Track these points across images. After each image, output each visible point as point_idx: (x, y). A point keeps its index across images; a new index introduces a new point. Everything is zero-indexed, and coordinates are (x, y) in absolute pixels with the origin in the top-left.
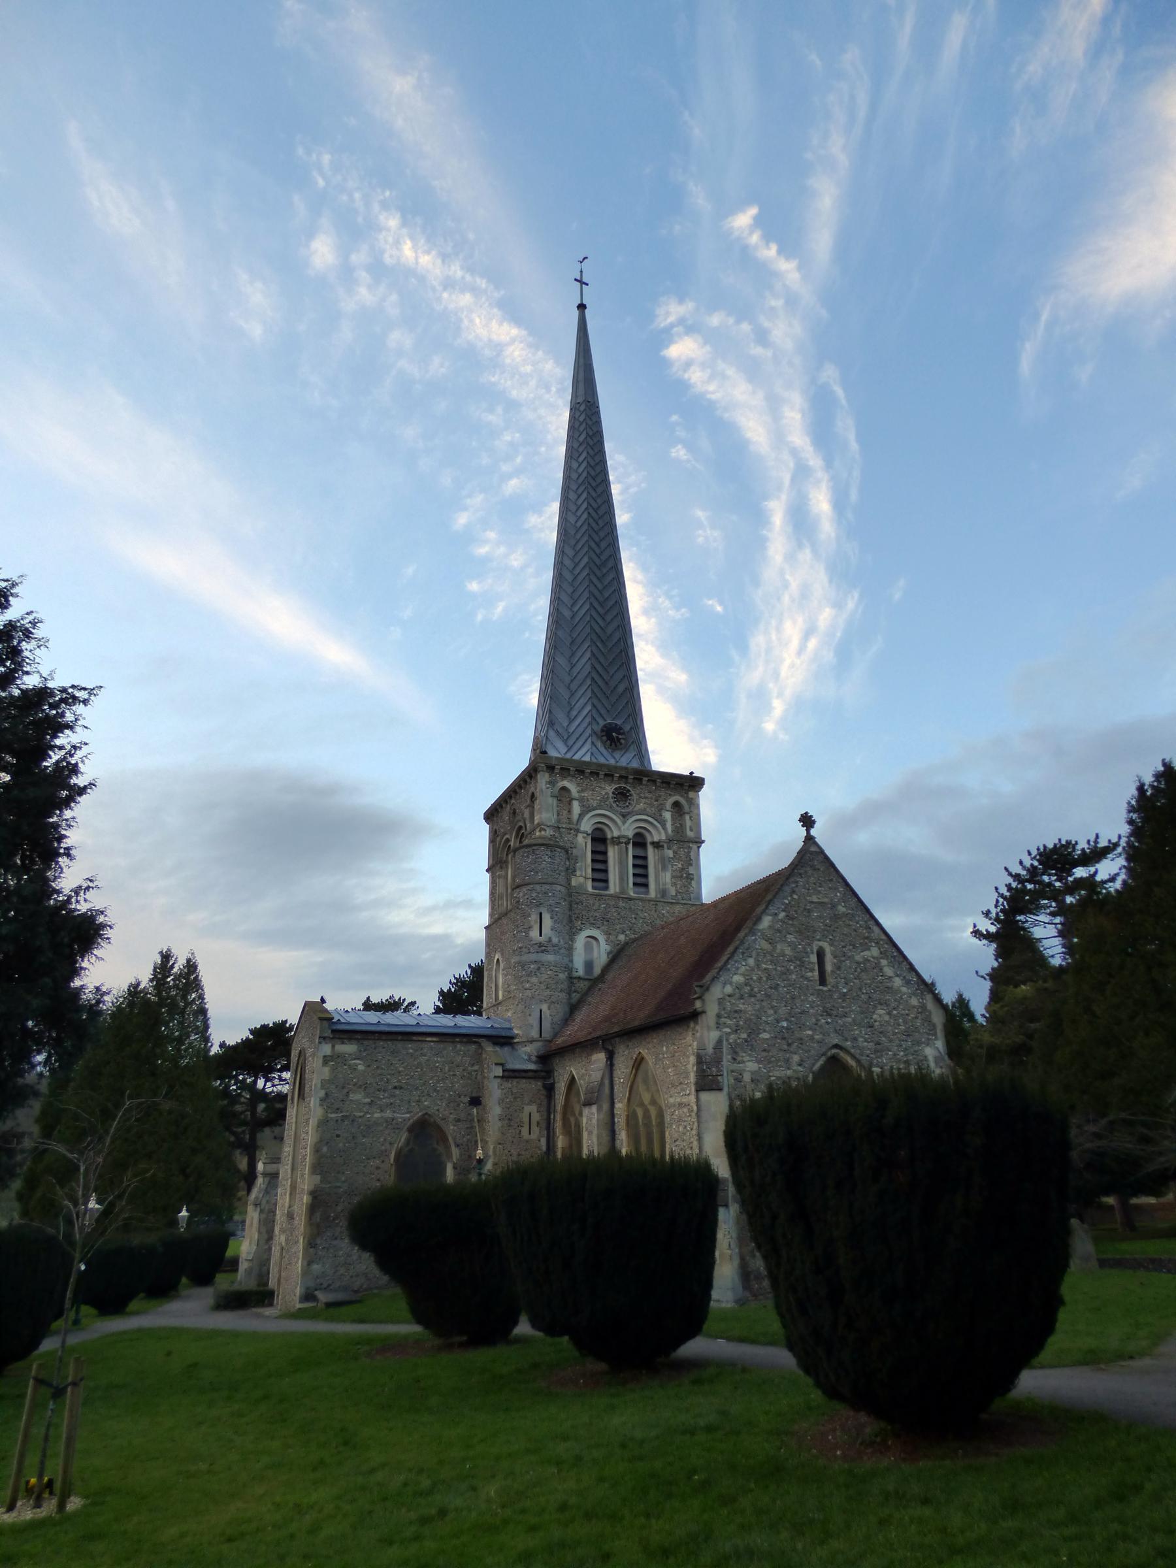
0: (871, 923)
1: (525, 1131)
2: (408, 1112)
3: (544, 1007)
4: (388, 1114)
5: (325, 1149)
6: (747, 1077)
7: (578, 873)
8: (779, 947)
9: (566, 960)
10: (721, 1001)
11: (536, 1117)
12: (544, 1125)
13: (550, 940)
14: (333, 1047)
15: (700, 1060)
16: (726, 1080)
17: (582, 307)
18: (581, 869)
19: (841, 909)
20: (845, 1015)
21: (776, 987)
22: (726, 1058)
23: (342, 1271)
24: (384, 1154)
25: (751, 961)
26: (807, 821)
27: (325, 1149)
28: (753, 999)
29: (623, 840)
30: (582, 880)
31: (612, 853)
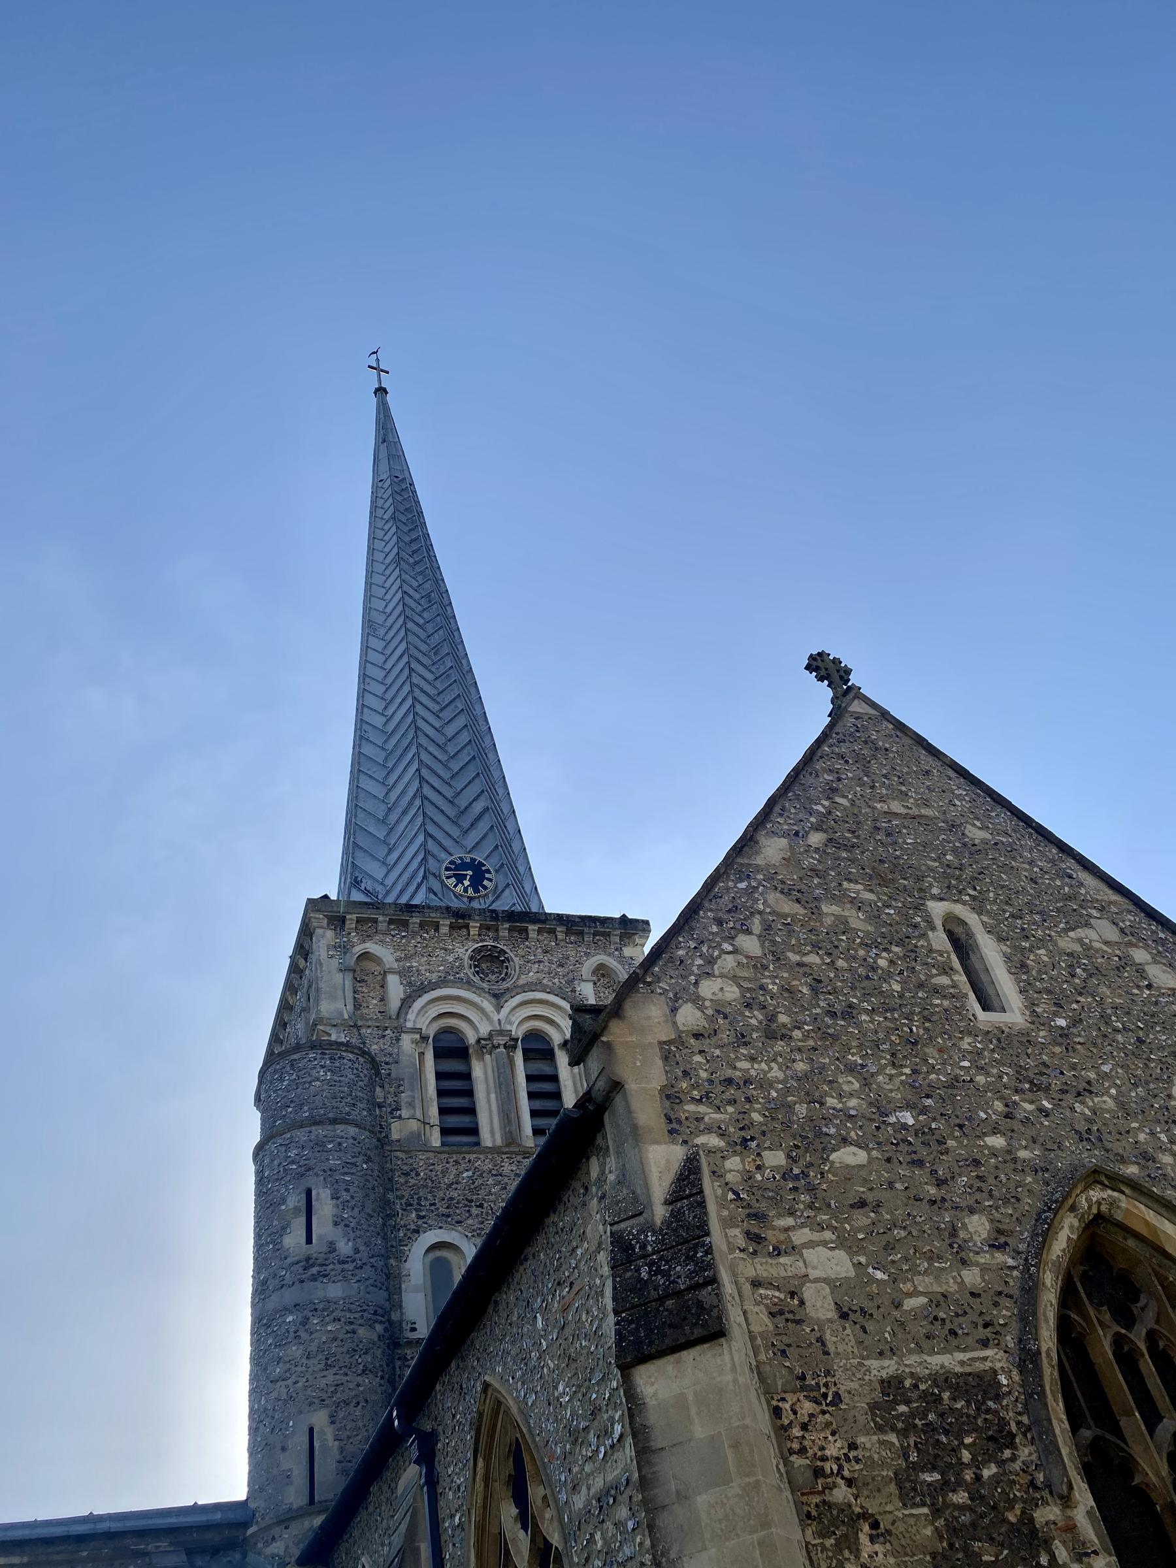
0: (1069, 864)
3: (320, 1419)
6: (820, 1305)
7: (405, 1113)
8: (829, 908)
9: (380, 1297)
10: (669, 1051)
15: (624, 1251)
16: (745, 1313)
17: (381, 391)
18: (411, 1105)
19: (975, 833)
20: (1088, 1090)
21: (849, 1012)
22: (724, 1236)
25: (750, 944)
26: (823, 667)
28: (780, 1046)
29: (502, 1040)
30: (414, 1125)
31: (481, 1071)
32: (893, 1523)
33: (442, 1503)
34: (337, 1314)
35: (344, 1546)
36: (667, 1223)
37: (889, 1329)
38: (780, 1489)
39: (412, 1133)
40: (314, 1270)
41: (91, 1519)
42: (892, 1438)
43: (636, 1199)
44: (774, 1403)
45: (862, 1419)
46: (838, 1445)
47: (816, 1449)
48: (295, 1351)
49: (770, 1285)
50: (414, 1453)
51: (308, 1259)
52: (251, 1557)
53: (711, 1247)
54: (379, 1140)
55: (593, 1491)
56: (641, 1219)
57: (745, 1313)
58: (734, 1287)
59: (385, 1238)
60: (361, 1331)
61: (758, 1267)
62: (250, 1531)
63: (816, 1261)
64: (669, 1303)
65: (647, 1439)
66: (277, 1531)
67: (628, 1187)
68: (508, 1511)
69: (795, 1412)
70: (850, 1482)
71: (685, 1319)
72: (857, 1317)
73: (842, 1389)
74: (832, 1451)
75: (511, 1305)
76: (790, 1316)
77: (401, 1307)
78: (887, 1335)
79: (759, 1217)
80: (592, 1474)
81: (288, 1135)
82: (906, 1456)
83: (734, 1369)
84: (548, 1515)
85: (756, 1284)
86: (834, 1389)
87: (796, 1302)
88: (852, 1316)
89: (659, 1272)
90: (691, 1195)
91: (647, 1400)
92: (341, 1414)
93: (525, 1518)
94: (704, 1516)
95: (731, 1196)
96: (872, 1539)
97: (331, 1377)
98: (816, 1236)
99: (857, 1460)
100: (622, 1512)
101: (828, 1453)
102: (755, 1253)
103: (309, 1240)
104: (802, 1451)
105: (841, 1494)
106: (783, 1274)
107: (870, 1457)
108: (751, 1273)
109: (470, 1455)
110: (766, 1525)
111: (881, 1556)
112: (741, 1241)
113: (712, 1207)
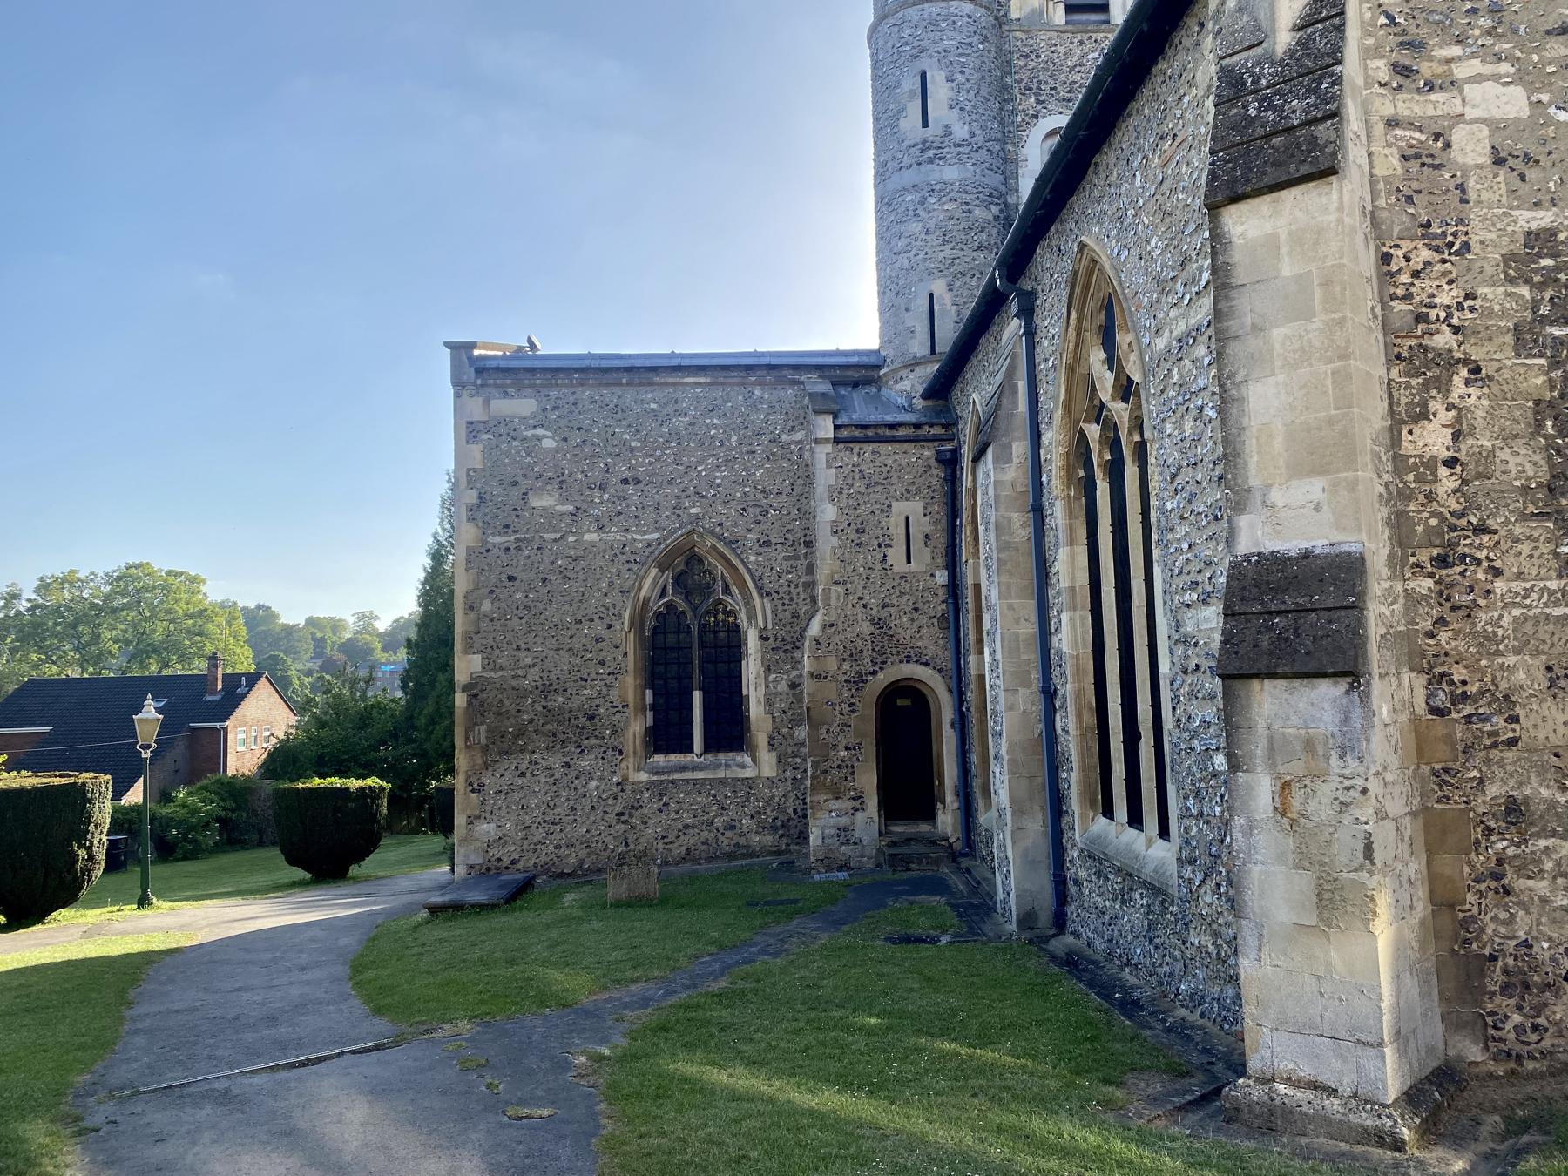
1: (896, 555)
2: (658, 529)
3: (939, 287)
4: (614, 535)
5: (486, 606)
6: (1470, 148)
9: (995, 180)
11: (921, 525)
12: (941, 541)
13: (948, 131)
14: (486, 402)
15: (1232, 86)
22: (1361, 66)
23: (540, 834)
24: (608, 616)
27: (486, 606)
32: (1500, 369)
33: (1038, 350)
34: (954, 195)
35: (959, 386)
36: (1291, 53)
37: (1556, 177)
38: (1370, 329)
39: (1033, 11)
40: (931, 153)
41: (755, 354)
42: (1525, 291)
43: (1258, 27)
44: (1385, 249)
45: (1489, 270)
46: (1453, 293)
47: (1424, 296)
48: (915, 227)
49: (1411, 125)
50: (1014, 308)
51: (924, 142)
52: (884, 391)
53: (1340, 77)
54: (996, 18)
55: (1175, 333)
56: (1259, 50)
57: (1370, 155)
58: (1362, 125)
59: (1002, 122)
60: (977, 212)
61: (1400, 104)
62: (882, 372)
63: (1479, 99)
64: (1276, 140)
65: (1228, 276)
66: (903, 373)
67: (1249, 14)
68: (1097, 356)
69: (1408, 260)
70: (1456, 330)
71: (1293, 156)
72: (1518, 164)
73: (1474, 241)
74: (1444, 298)
75: (1111, 166)
76: (1429, 160)
77: (1017, 191)
78: (1551, 184)
79: (1416, 46)
80: (1176, 319)
81: (900, 15)
82: (1535, 310)
83: (1341, 208)
84: (1132, 357)
85: (1392, 123)
86: (1464, 238)
87: (1440, 144)
88: (1511, 162)
89: (1271, 106)
90: (1328, 18)
91: (1235, 240)
92: (958, 284)
93: (1112, 361)
94: (1277, 347)
95: (1383, 20)
96: (1468, 383)
97: (948, 251)
98: (1487, 69)
99: (1472, 309)
100: (1201, 351)
101: (1437, 301)
102: (1400, 87)
103: (925, 124)
104: (1408, 297)
105: (1444, 339)
106: (1431, 112)
107: (1491, 309)
108: (1388, 111)
109: (1065, 309)
110: (1344, 356)
111: (1474, 398)
112: (1384, 75)
113: (1353, 32)
